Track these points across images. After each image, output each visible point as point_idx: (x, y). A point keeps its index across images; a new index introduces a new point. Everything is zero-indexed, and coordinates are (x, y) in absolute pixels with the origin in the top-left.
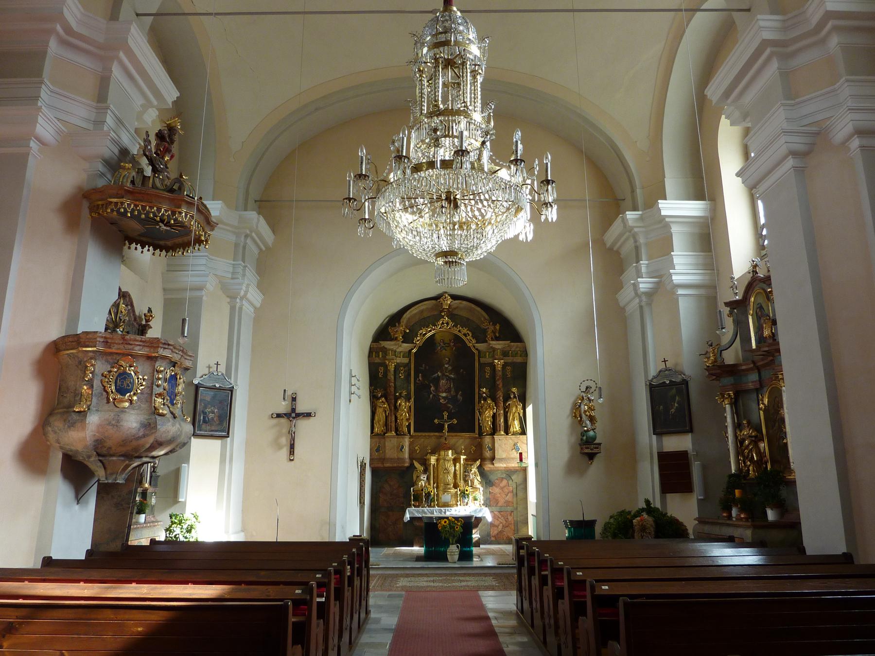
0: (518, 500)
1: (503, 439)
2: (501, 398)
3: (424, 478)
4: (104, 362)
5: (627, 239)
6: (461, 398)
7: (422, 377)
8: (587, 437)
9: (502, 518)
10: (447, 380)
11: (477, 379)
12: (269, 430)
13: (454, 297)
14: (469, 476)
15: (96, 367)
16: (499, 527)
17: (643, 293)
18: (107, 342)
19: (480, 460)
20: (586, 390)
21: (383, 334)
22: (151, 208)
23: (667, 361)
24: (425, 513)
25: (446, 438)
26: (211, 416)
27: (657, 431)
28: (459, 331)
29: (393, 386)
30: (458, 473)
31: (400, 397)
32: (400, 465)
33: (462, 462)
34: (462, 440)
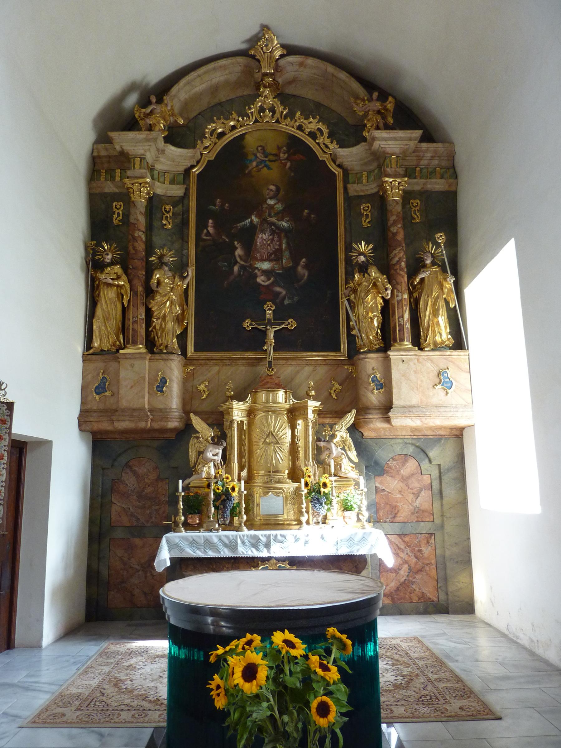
0: (446, 507)
1: (410, 360)
2: (403, 264)
6: (306, 275)
7: (215, 227)
9: (408, 550)
10: (273, 233)
14: (329, 449)
16: (402, 572)
19: (354, 411)
24: (213, 546)
25: (270, 363)
28: (300, 128)
29: (144, 238)
30: (301, 443)
31: (161, 263)
33: (311, 416)
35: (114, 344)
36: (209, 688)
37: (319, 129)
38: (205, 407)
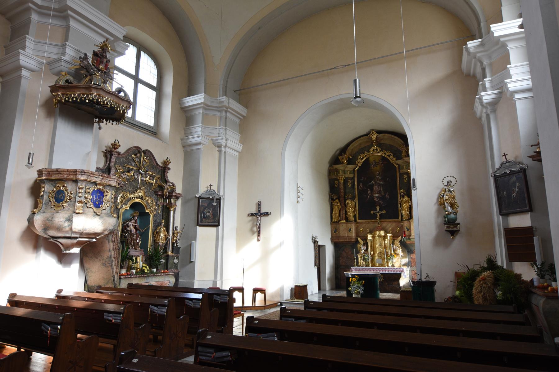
3: (364, 248)
4: (50, 185)
5: (475, 65)
6: (388, 197)
7: (362, 185)
8: (448, 218)
11: (398, 184)
12: (248, 223)
13: (379, 132)
15: (46, 188)
17: (487, 103)
18: (50, 174)
20: (448, 184)
21: (335, 161)
22: (75, 94)
23: (507, 155)
26: (208, 214)
27: (503, 212)
28: (385, 154)
32: (349, 240)
33: (389, 238)
34: (390, 224)
35: (338, 220)
36: (108, 121)
37: (390, 154)
38: (362, 235)
